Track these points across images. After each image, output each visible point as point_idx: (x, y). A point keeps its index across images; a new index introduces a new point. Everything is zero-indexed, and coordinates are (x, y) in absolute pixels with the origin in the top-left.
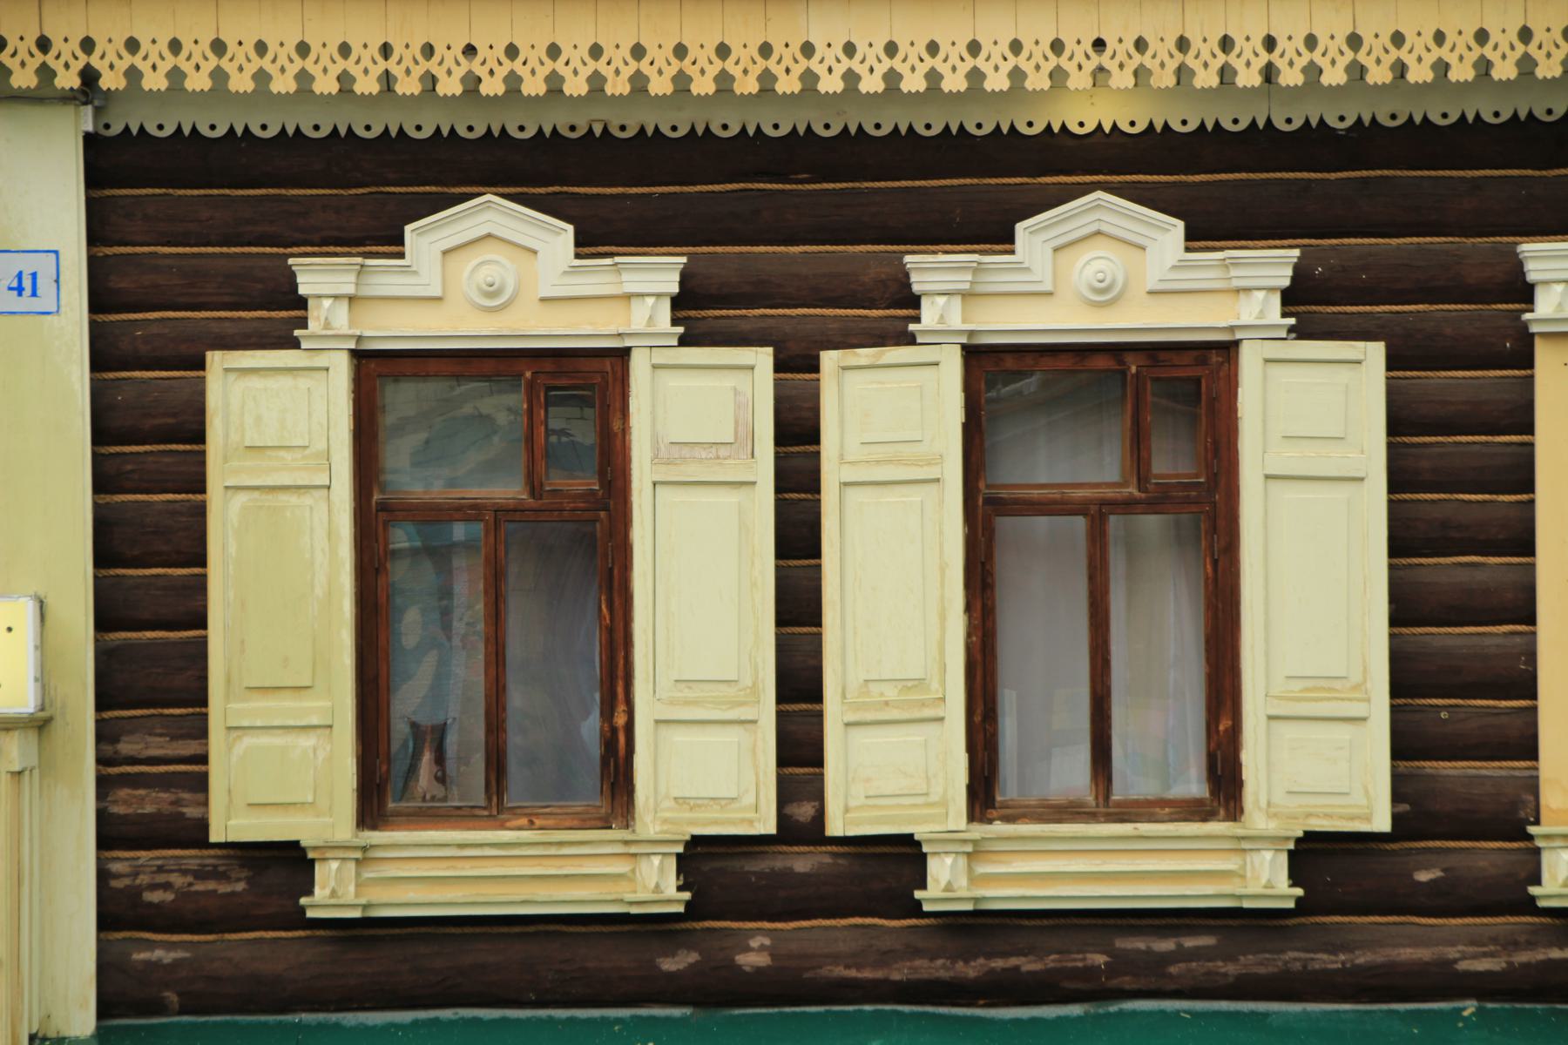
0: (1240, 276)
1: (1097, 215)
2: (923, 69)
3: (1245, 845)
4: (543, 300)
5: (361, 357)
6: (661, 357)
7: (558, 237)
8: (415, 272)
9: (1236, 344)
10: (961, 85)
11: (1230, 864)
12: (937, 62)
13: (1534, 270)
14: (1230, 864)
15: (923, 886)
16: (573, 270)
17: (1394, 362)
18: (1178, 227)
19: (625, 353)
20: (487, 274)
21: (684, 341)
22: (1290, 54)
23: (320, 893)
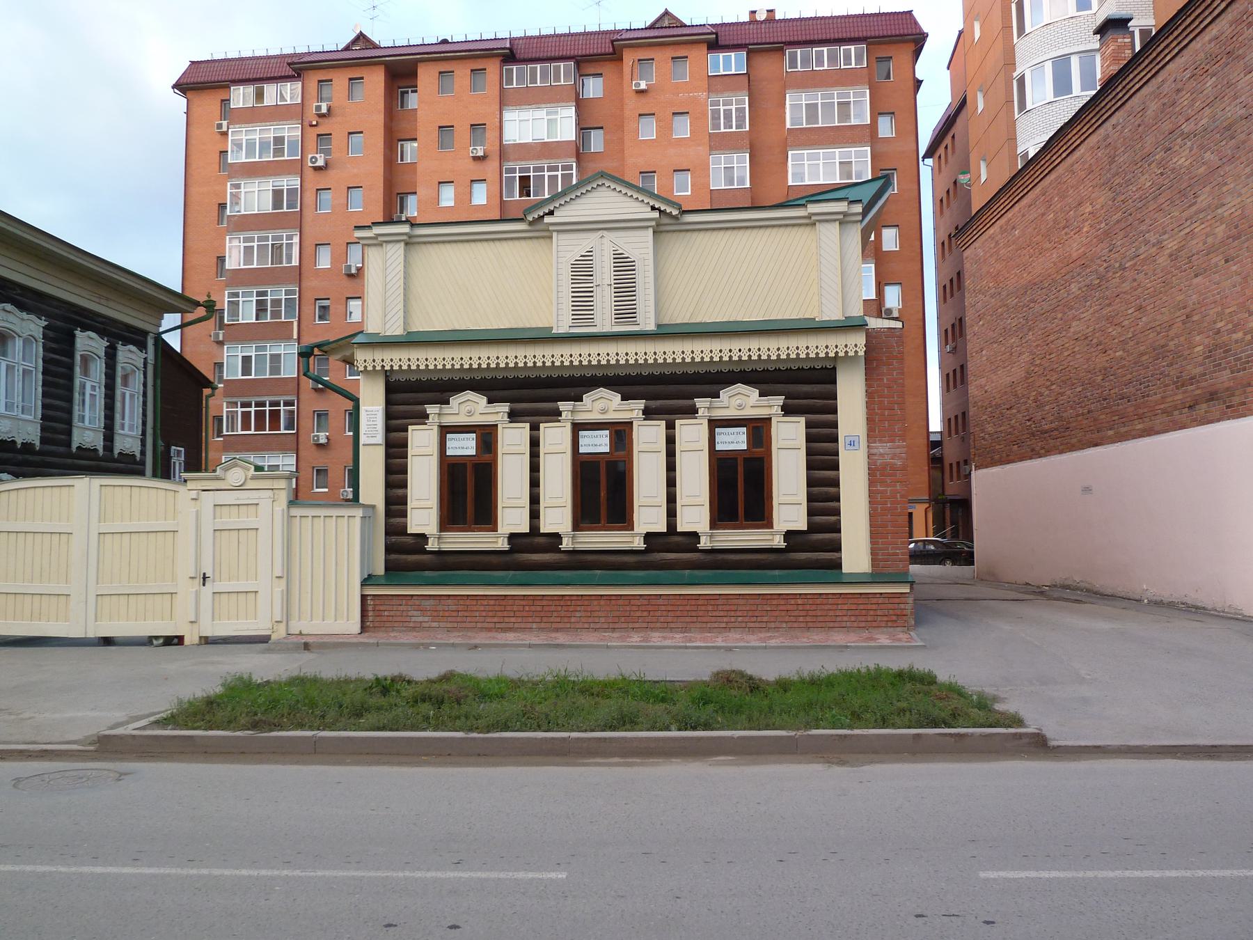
0: (772, 403)
1: (739, 389)
2: (532, 361)
3: (633, 536)
4: (480, 414)
5: (710, 421)
6: (641, 423)
7: (483, 400)
8: (452, 408)
9: (771, 418)
10: (559, 364)
11: (770, 537)
12: (454, 362)
13: (698, 405)
14: (770, 537)
15: (427, 545)
16: (486, 407)
18: (485, 399)
19: (497, 425)
20: (738, 402)
21: (511, 422)
22: (812, 350)
23: (430, 545)
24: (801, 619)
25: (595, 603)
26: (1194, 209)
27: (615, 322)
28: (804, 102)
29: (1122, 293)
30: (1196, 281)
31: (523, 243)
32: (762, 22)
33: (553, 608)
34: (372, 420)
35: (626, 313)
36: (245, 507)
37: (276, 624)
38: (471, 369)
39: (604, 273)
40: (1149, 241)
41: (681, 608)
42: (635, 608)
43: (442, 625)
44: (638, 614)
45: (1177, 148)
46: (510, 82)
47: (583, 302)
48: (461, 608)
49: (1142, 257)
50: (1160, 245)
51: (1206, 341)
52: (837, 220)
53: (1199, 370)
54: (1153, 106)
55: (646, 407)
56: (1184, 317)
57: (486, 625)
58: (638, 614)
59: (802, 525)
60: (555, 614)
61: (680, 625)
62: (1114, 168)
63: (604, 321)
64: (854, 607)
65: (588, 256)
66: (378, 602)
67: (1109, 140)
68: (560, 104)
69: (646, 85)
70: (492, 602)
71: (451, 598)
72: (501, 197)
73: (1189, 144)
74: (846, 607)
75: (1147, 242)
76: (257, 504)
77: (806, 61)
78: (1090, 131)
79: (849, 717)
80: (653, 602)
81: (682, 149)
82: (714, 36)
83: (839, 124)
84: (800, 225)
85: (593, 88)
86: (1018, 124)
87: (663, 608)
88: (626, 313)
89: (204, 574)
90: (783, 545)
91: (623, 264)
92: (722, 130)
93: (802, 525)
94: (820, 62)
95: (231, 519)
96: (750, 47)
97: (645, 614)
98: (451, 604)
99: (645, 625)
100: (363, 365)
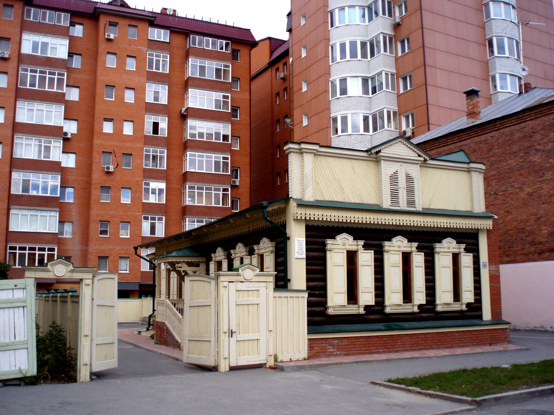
17: (425, 256)
24: (476, 341)
25: (405, 338)
26: (542, 179)
27: (407, 206)
28: (198, 64)
29: (495, 204)
30: (543, 206)
31: (363, 162)
32: (170, 15)
33: (388, 341)
34: (300, 245)
35: (411, 203)
36: (252, 292)
37: (269, 357)
38: (437, 227)
39: (402, 183)
40: (514, 186)
41: (436, 338)
42: (420, 339)
43: (342, 353)
44: (421, 342)
45: (532, 154)
46: (29, 16)
47: (394, 195)
48: (350, 343)
49: (509, 192)
50: (521, 189)
51: (549, 229)
52: (419, 164)
53: (544, 240)
54: (517, 135)
55: (364, 243)
56: (536, 219)
57: (361, 352)
58: (421, 342)
59: (472, 301)
60: (390, 344)
61: (436, 347)
62: (491, 153)
63: (403, 205)
64: (492, 335)
65: (396, 173)
66: (312, 342)
67: (487, 142)
68: (60, 37)
69: (114, 36)
70: (364, 340)
71: (346, 338)
72: (17, 84)
73: (540, 154)
74: (489, 335)
75: (512, 186)
76: (259, 290)
77: (200, 43)
78: (476, 135)
79: (527, 380)
80: (498, 332)
81: (132, 77)
82: (154, 19)
83: (216, 79)
84: (464, 171)
85: (78, 31)
86: (332, 103)
87: (430, 339)
88: (411, 203)
89: (232, 330)
90: (364, 312)
91: (409, 179)
92: (154, 70)
93: (472, 301)
94: (208, 45)
95: (244, 299)
96: (172, 29)
97: (424, 342)
98: (345, 342)
99: (423, 347)
100: (300, 216)
